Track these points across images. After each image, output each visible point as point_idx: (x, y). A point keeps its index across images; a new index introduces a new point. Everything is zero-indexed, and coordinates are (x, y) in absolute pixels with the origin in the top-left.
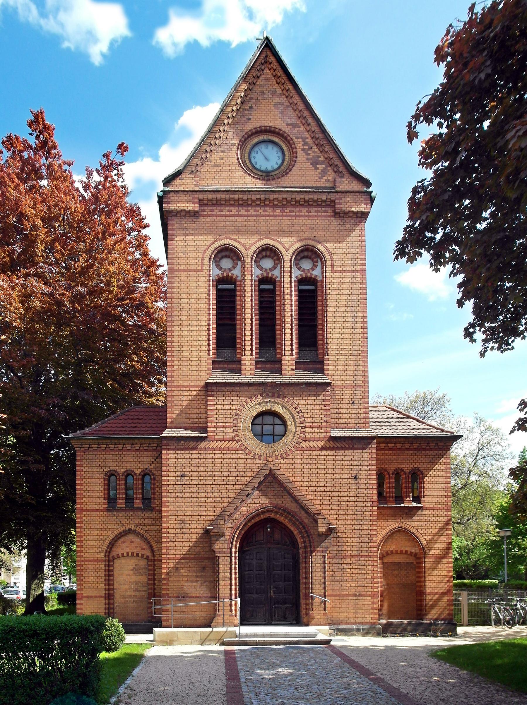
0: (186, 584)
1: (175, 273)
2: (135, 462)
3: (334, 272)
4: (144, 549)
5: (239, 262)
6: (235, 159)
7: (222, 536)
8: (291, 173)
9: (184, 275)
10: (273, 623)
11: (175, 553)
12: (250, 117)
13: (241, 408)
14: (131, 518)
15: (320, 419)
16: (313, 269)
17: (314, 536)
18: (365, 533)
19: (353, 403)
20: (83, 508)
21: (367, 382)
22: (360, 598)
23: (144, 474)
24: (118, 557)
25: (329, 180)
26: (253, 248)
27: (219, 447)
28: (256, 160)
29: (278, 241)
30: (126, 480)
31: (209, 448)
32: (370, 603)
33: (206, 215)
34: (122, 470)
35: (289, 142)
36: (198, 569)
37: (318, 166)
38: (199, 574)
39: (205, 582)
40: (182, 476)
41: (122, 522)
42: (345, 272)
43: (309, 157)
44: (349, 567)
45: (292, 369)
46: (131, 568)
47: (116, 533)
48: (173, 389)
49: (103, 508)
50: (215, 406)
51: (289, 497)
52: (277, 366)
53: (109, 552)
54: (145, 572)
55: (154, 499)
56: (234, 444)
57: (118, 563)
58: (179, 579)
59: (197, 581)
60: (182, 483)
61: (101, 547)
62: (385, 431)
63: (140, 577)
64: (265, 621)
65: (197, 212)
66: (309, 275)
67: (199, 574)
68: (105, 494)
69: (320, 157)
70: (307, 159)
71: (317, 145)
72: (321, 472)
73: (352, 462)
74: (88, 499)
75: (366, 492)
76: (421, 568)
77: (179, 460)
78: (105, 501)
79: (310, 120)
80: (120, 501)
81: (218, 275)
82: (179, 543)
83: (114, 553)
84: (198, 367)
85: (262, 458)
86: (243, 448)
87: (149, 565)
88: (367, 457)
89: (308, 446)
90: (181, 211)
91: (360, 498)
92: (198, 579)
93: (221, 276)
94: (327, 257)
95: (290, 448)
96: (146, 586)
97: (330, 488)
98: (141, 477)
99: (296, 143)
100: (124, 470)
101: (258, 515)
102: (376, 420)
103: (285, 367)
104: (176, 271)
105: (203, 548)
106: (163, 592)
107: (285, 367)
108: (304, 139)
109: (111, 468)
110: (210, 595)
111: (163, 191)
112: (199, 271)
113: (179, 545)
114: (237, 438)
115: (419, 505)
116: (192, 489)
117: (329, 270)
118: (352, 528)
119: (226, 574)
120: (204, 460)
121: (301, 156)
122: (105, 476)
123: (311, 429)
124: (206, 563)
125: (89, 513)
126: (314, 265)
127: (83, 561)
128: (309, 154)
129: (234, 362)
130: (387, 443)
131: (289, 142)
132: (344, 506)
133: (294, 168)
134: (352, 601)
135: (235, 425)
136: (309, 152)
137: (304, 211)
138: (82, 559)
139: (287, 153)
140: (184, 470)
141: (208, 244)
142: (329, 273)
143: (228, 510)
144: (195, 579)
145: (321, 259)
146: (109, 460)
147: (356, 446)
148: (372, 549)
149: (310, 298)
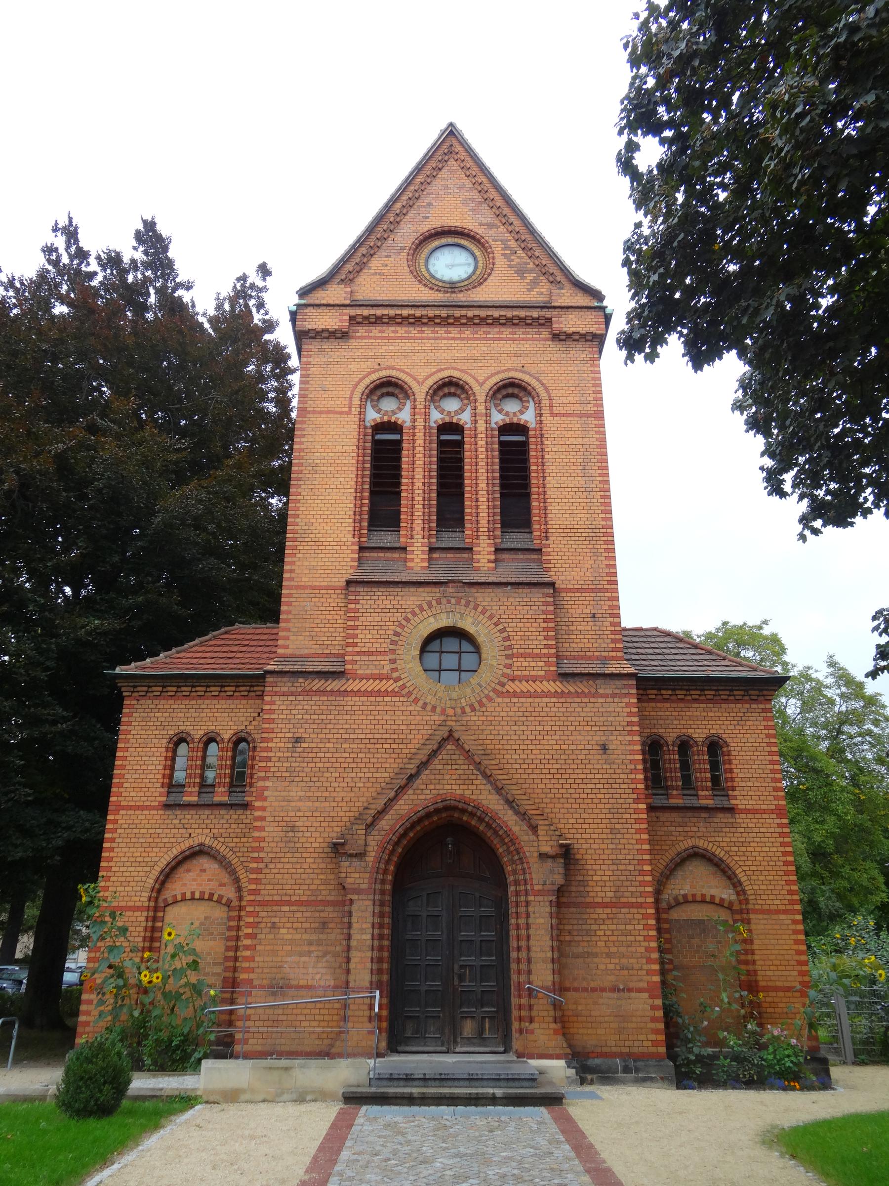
0: (289, 959)
2: (223, 717)
5: (408, 402)
9: (321, 419)
10: (457, 1050)
11: (272, 892)
13: (404, 623)
14: (206, 821)
16: (522, 413)
17: (530, 860)
18: (628, 857)
21: (616, 583)
22: (626, 994)
23: (239, 740)
26: (430, 382)
28: (436, 268)
30: (205, 749)
31: (345, 691)
33: (359, 338)
35: (483, 246)
36: (313, 925)
38: (314, 937)
39: (325, 954)
40: (297, 742)
41: (189, 831)
44: (602, 927)
51: (484, 782)
52: (465, 556)
53: (159, 891)
54: (223, 934)
56: (391, 686)
57: (173, 914)
58: (276, 948)
59: (309, 953)
61: (144, 879)
63: (212, 943)
64: (442, 1045)
65: (347, 333)
66: (515, 420)
67: (314, 937)
68: (164, 777)
70: (509, 266)
73: (596, 719)
75: (624, 776)
78: (162, 790)
79: (512, 218)
81: (374, 420)
82: (282, 871)
83: (167, 895)
85: (438, 710)
86: (404, 692)
87: (230, 918)
89: (518, 691)
90: (323, 331)
91: (615, 786)
92: (312, 948)
93: (379, 421)
96: (220, 964)
97: (559, 766)
98: (230, 745)
101: (428, 815)
102: (639, 651)
103: (478, 557)
104: (309, 412)
105: (324, 883)
106: (243, 976)
107: (478, 557)
109: (181, 728)
110: (332, 983)
111: (298, 305)
113: (280, 876)
114: (395, 675)
116: (313, 765)
117: (546, 414)
119: (364, 937)
121: (500, 263)
123: (522, 659)
124: (329, 913)
125: (130, 812)
126: (523, 407)
128: (513, 260)
129: (396, 548)
131: (483, 246)
132: (586, 801)
135: (393, 652)
137: (506, 332)
139: (481, 260)
140: (301, 730)
142: (547, 419)
144: (306, 948)
147: (601, 691)
149: (515, 454)
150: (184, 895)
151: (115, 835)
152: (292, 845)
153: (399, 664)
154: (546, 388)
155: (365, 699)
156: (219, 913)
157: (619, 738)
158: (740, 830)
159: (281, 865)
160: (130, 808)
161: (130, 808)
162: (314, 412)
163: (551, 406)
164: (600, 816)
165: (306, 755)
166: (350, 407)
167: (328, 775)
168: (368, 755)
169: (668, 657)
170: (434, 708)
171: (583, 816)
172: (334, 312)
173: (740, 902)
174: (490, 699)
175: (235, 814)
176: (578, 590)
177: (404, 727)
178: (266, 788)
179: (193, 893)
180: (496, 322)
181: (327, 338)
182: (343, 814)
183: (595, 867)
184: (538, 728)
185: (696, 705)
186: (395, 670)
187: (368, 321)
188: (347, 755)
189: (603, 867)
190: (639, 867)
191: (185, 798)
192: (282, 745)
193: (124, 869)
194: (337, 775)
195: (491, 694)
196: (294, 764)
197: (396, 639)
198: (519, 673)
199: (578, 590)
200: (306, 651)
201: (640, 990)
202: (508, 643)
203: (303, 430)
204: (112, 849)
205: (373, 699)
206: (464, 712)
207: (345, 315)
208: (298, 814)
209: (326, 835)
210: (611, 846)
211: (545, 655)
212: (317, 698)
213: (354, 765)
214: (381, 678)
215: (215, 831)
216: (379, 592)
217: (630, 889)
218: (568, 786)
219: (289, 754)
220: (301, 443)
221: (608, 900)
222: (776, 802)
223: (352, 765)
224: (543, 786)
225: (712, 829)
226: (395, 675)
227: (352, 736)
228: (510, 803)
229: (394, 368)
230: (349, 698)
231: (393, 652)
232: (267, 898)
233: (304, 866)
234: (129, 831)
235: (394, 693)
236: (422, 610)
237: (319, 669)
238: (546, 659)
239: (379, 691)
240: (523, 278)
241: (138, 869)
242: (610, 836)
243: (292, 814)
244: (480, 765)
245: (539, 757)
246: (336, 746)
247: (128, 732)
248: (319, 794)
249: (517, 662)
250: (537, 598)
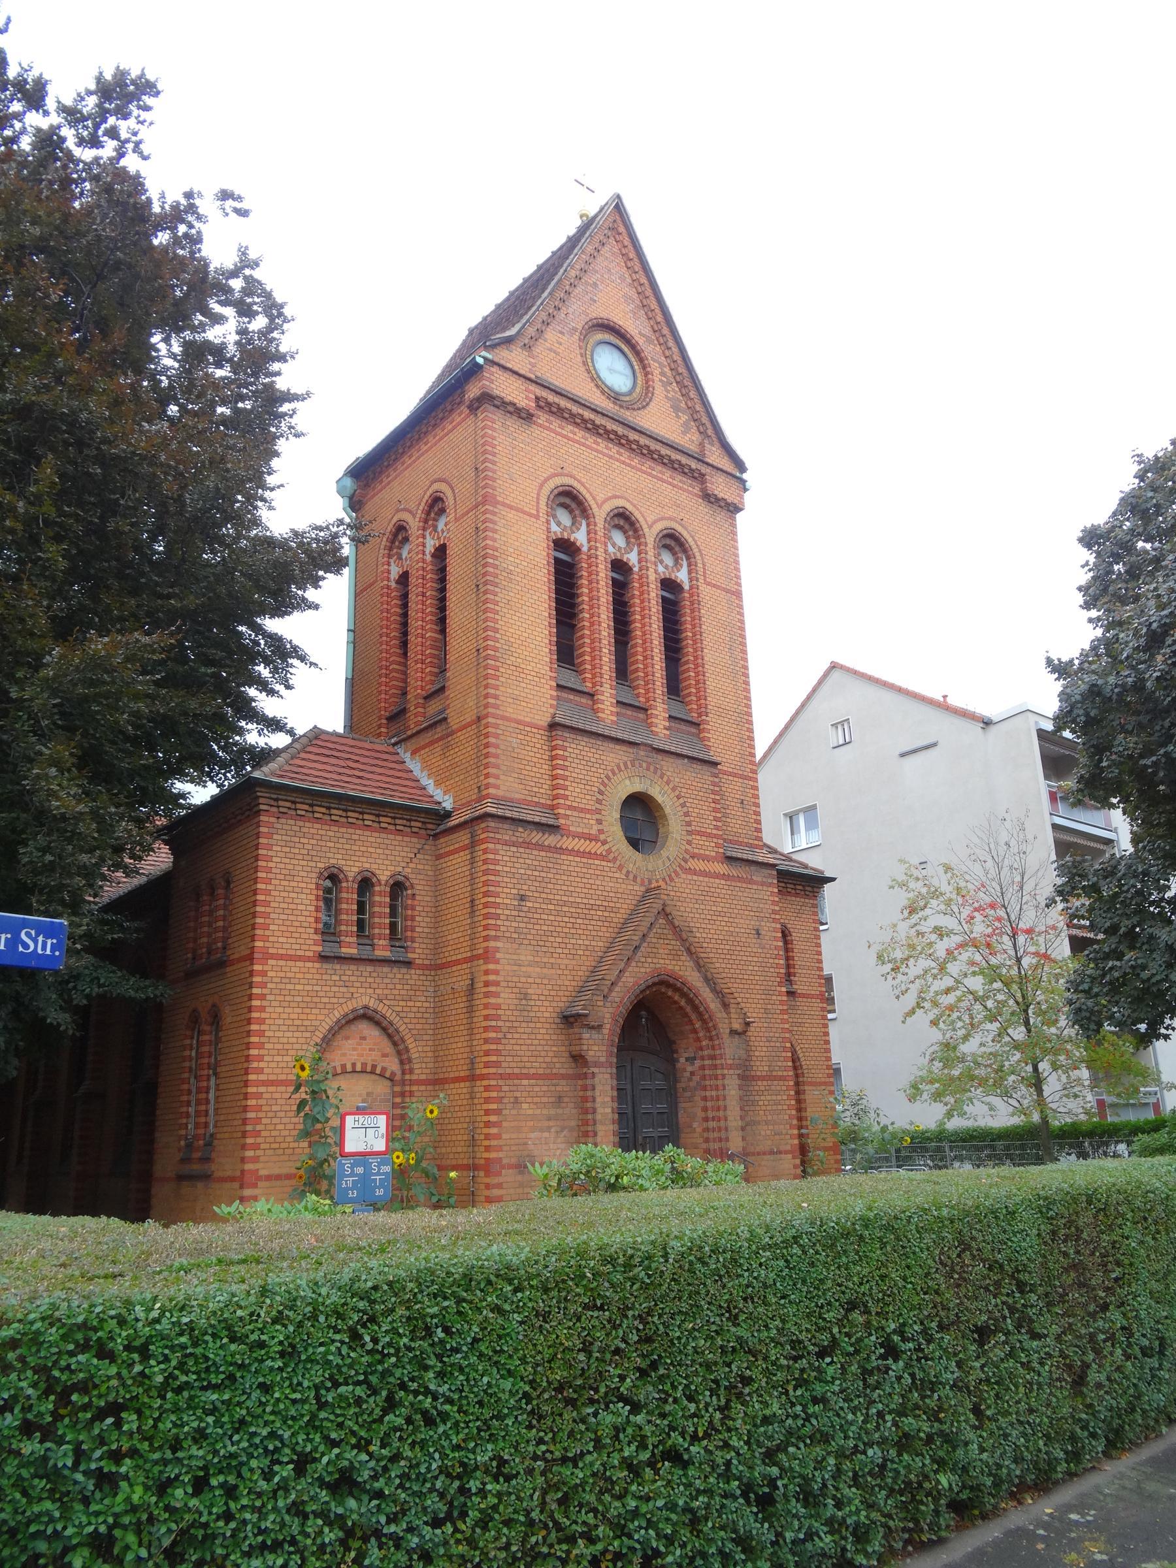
0: (532, 1135)
3: (708, 584)
4: (385, 1055)
38: (552, 1112)
55: (413, 940)
59: (549, 1129)
67: (552, 1112)
112: (530, 515)
114: (602, 837)
124: (563, 1086)
135: (598, 811)
138: (262, 1077)
144: (546, 1124)
150: (343, 1066)
151: (265, 991)
153: (604, 827)
156: (382, 1088)
160: (281, 957)
161: (281, 957)
162: (504, 504)
169: (342, 763)
170: (635, 877)
172: (519, 383)
173: (403, 1073)
175: (399, 973)
178: (497, 949)
179: (354, 1065)
180: (661, 460)
187: (558, 412)
193: (280, 1034)
200: (517, 796)
201: (786, 1152)
204: (262, 1009)
207: (530, 392)
211: (715, 836)
215: (378, 991)
216: (584, 741)
226: (602, 837)
228: (707, 980)
231: (598, 811)
232: (509, 1071)
235: (602, 857)
237: (537, 819)
240: (678, 417)
243: (523, 980)
247: (269, 859)
250: (705, 773)
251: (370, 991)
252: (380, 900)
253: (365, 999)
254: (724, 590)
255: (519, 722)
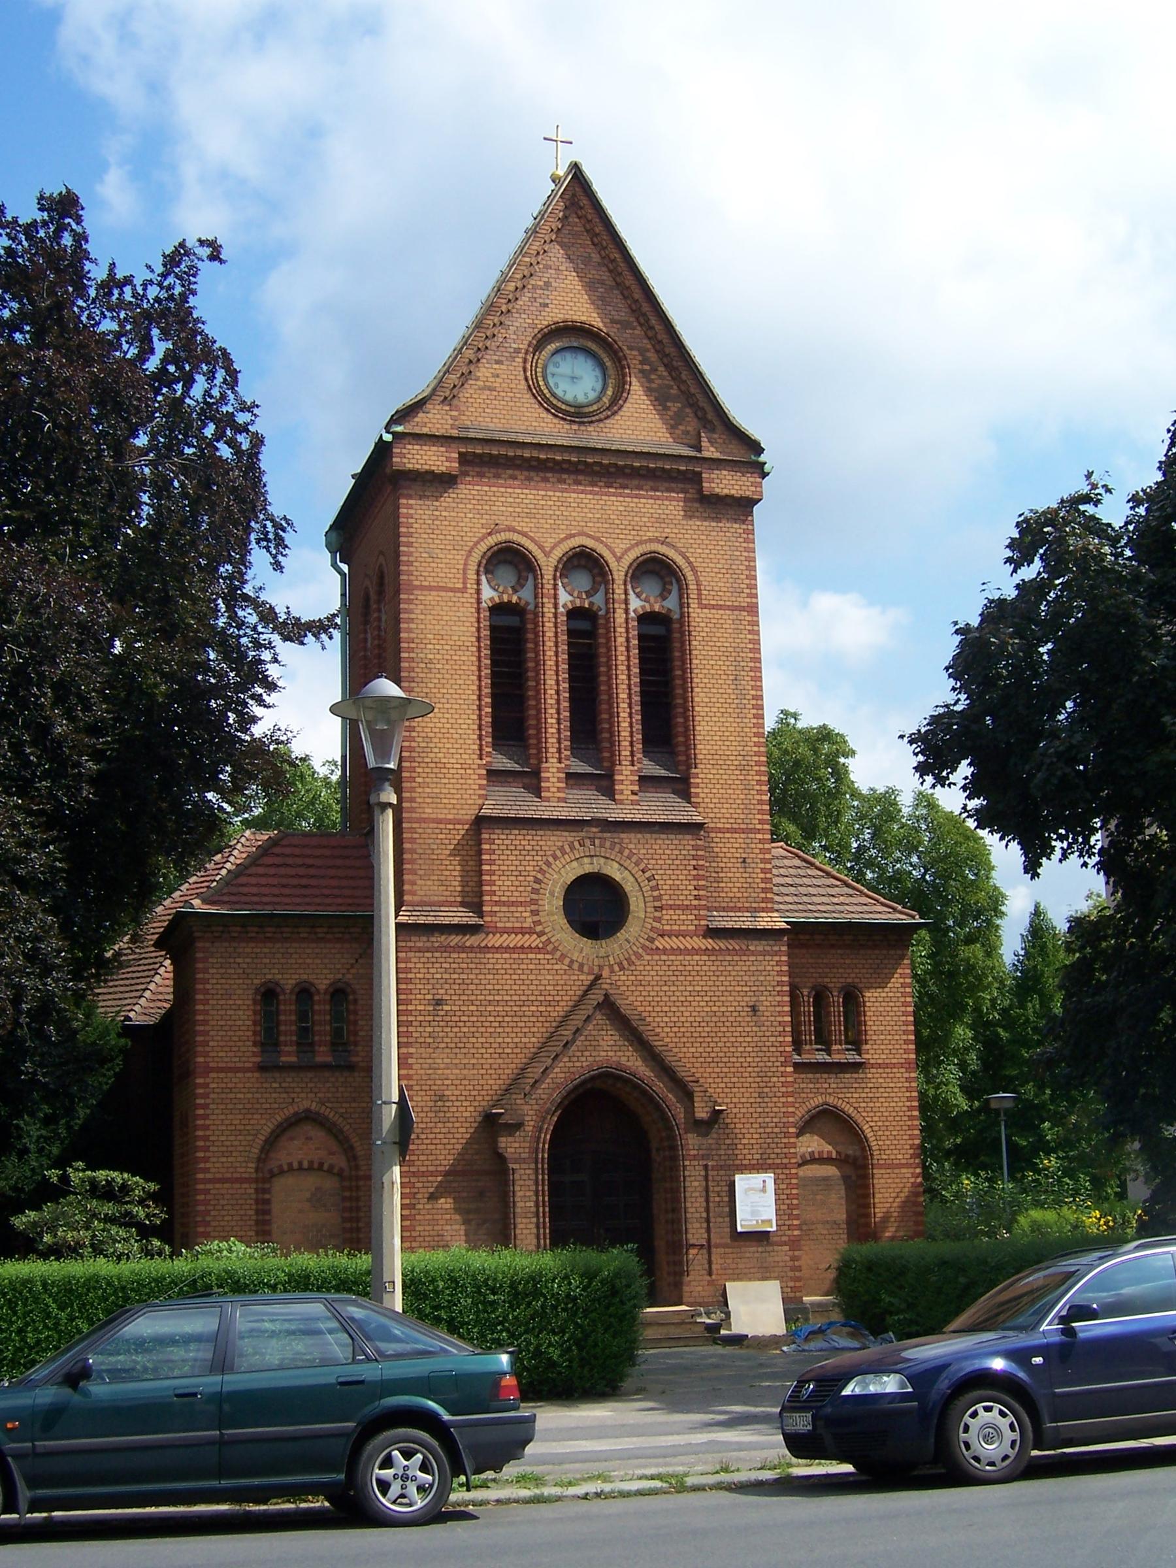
1: (416, 592)
3: (702, 606)
4: (333, 1154)
6: (522, 377)
7: (519, 1126)
8: (621, 413)
9: (431, 597)
11: (426, 1163)
12: (547, 301)
13: (544, 867)
15: (687, 894)
19: (744, 862)
20: (211, 1065)
24: (282, 1172)
25: (688, 432)
26: (558, 553)
27: (505, 945)
29: (602, 542)
31: (486, 947)
32: (788, 1258)
34: (290, 982)
37: (669, 404)
40: (437, 1004)
41: (293, 1095)
42: (720, 607)
43: (654, 385)
45: (634, 793)
46: (308, 1195)
47: (279, 1119)
48: (414, 825)
49: (251, 1065)
50: (498, 862)
55: (356, 1044)
60: (437, 1018)
61: (248, 1148)
62: (790, 907)
69: (671, 387)
71: (665, 366)
72: (691, 999)
73: (746, 978)
74: (221, 1044)
76: (867, 1187)
77: (431, 971)
79: (653, 321)
80: (287, 1049)
81: (492, 599)
83: (273, 1165)
84: (461, 781)
85: (586, 969)
86: (550, 948)
88: (770, 969)
89: (668, 947)
90: (427, 472)
92: (471, 1217)
93: (497, 600)
94: (690, 576)
95: (635, 948)
99: (629, 357)
100: (294, 982)
103: (621, 787)
107: (621, 787)
108: (642, 351)
113: (433, 1147)
114: (539, 929)
115: (858, 1059)
116: (457, 1030)
117: (694, 604)
118: (751, 1110)
119: (528, 1204)
120: (477, 971)
122: (255, 994)
123: (672, 912)
125: (222, 1075)
126: (664, 589)
127: (210, 1181)
130: (797, 934)
133: (627, 405)
134: (756, 1255)
135: (534, 902)
136: (653, 377)
138: (208, 1176)
140: (441, 991)
141: (475, 539)
142: (694, 610)
143: (531, 1075)
145: (678, 581)
146: (265, 961)
148: (785, 1150)
150: (290, 1165)
152: (442, 1114)
154: (693, 569)
155: (507, 956)
157: (769, 999)
158: (870, 1085)
159: (433, 1136)
162: (422, 588)
163: (699, 594)
164: (749, 1080)
165: (448, 1018)
166: (464, 583)
167: (474, 1040)
168: (515, 1019)
170: (581, 965)
171: (733, 1080)
174: (639, 957)
176: (728, 830)
177: (551, 988)
179: (300, 1163)
181: (431, 481)
182: (492, 1082)
183: (743, 1131)
184: (689, 988)
185: (833, 951)
186: (539, 923)
188: (492, 1019)
189: (752, 1131)
190: (785, 1130)
191: (283, 1059)
192: (422, 1008)
194: (484, 1040)
195: (640, 950)
196: (437, 1029)
197: (537, 886)
198: (668, 927)
199: (728, 830)
202: (656, 893)
203: (411, 612)
205: (516, 956)
206: (612, 971)
208: (446, 1082)
209: (476, 1104)
210: (759, 1110)
212: (456, 955)
213: (500, 1030)
214: (523, 932)
217: (776, 1151)
218: (718, 1049)
219: (431, 1018)
220: (410, 630)
221: (755, 1162)
222: (906, 1056)
223: (498, 1030)
224: (693, 1050)
225: (841, 1085)
226: (539, 929)
227: (497, 998)
229: (514, 530)
230: (490, 955)
231: (534, 902)
233: (457, 1136)
234: (224, 1096)
236: (564, 853)
237: (456, 921)
238: (696, 912)
239: (522, 947)
241: (240, 1138)
242: (759, 1100)
244: (631, 1031)
245: (690, 1019)
246: (480, 1008)
248: (466, 1061)
249: (667, 915)
251: (312, 1095)
252: (321, 1007)
253: (306, 1103)
254: (729, 608)
255: (440, 821)
